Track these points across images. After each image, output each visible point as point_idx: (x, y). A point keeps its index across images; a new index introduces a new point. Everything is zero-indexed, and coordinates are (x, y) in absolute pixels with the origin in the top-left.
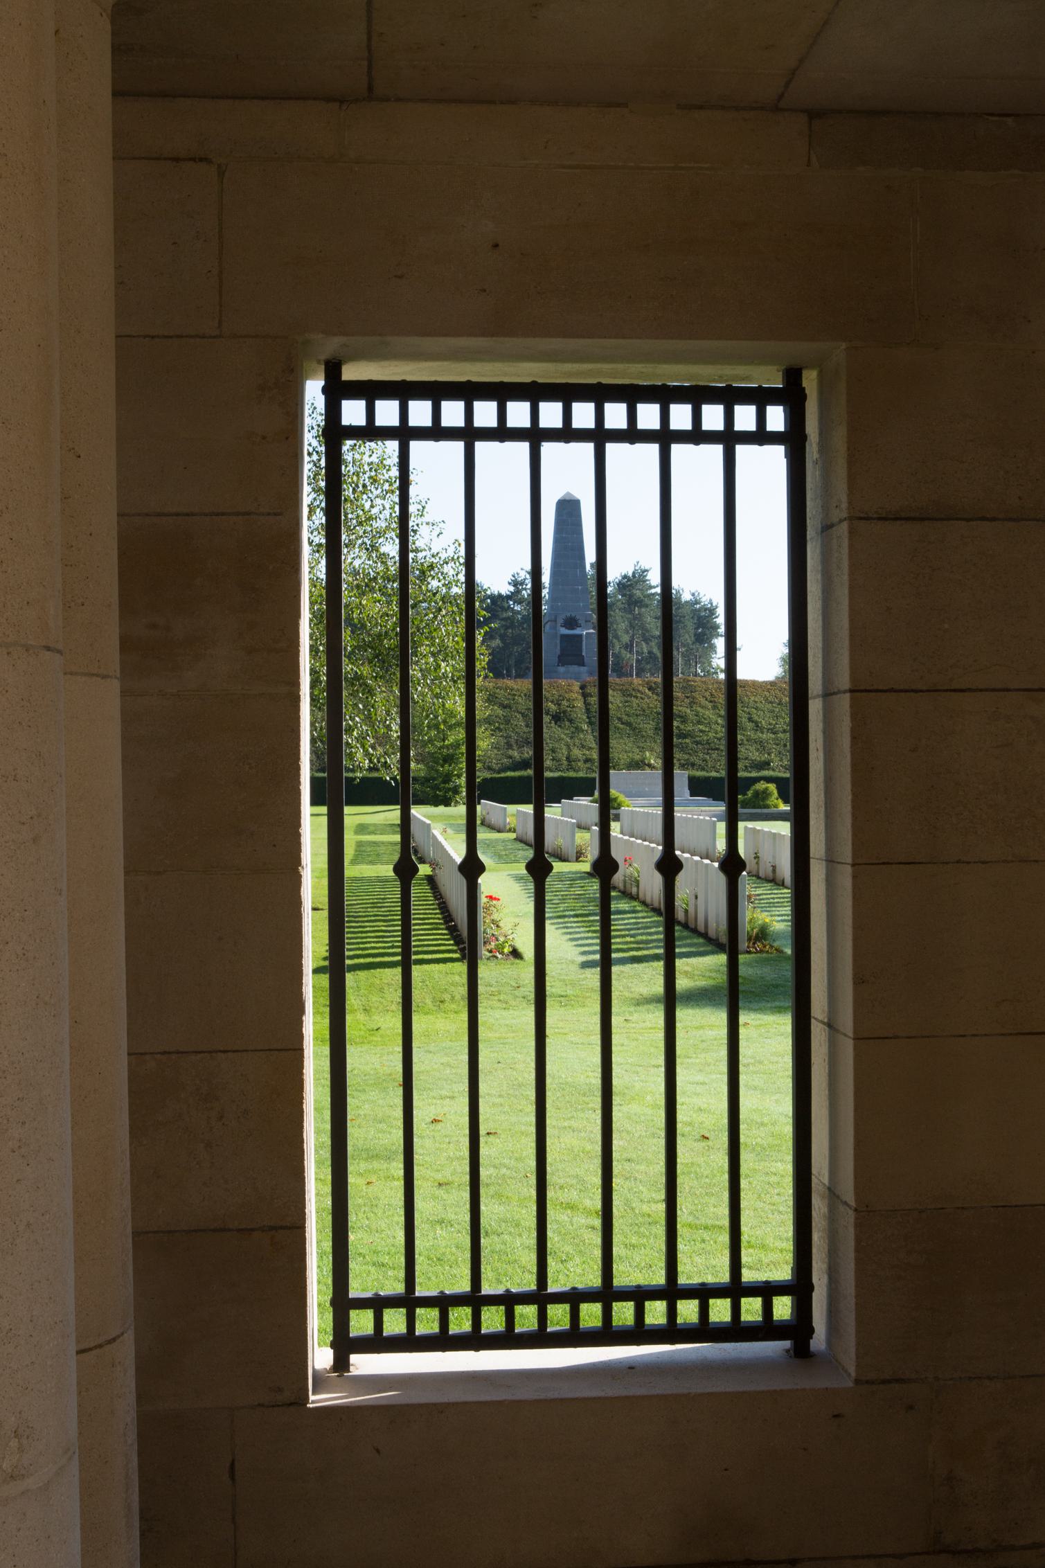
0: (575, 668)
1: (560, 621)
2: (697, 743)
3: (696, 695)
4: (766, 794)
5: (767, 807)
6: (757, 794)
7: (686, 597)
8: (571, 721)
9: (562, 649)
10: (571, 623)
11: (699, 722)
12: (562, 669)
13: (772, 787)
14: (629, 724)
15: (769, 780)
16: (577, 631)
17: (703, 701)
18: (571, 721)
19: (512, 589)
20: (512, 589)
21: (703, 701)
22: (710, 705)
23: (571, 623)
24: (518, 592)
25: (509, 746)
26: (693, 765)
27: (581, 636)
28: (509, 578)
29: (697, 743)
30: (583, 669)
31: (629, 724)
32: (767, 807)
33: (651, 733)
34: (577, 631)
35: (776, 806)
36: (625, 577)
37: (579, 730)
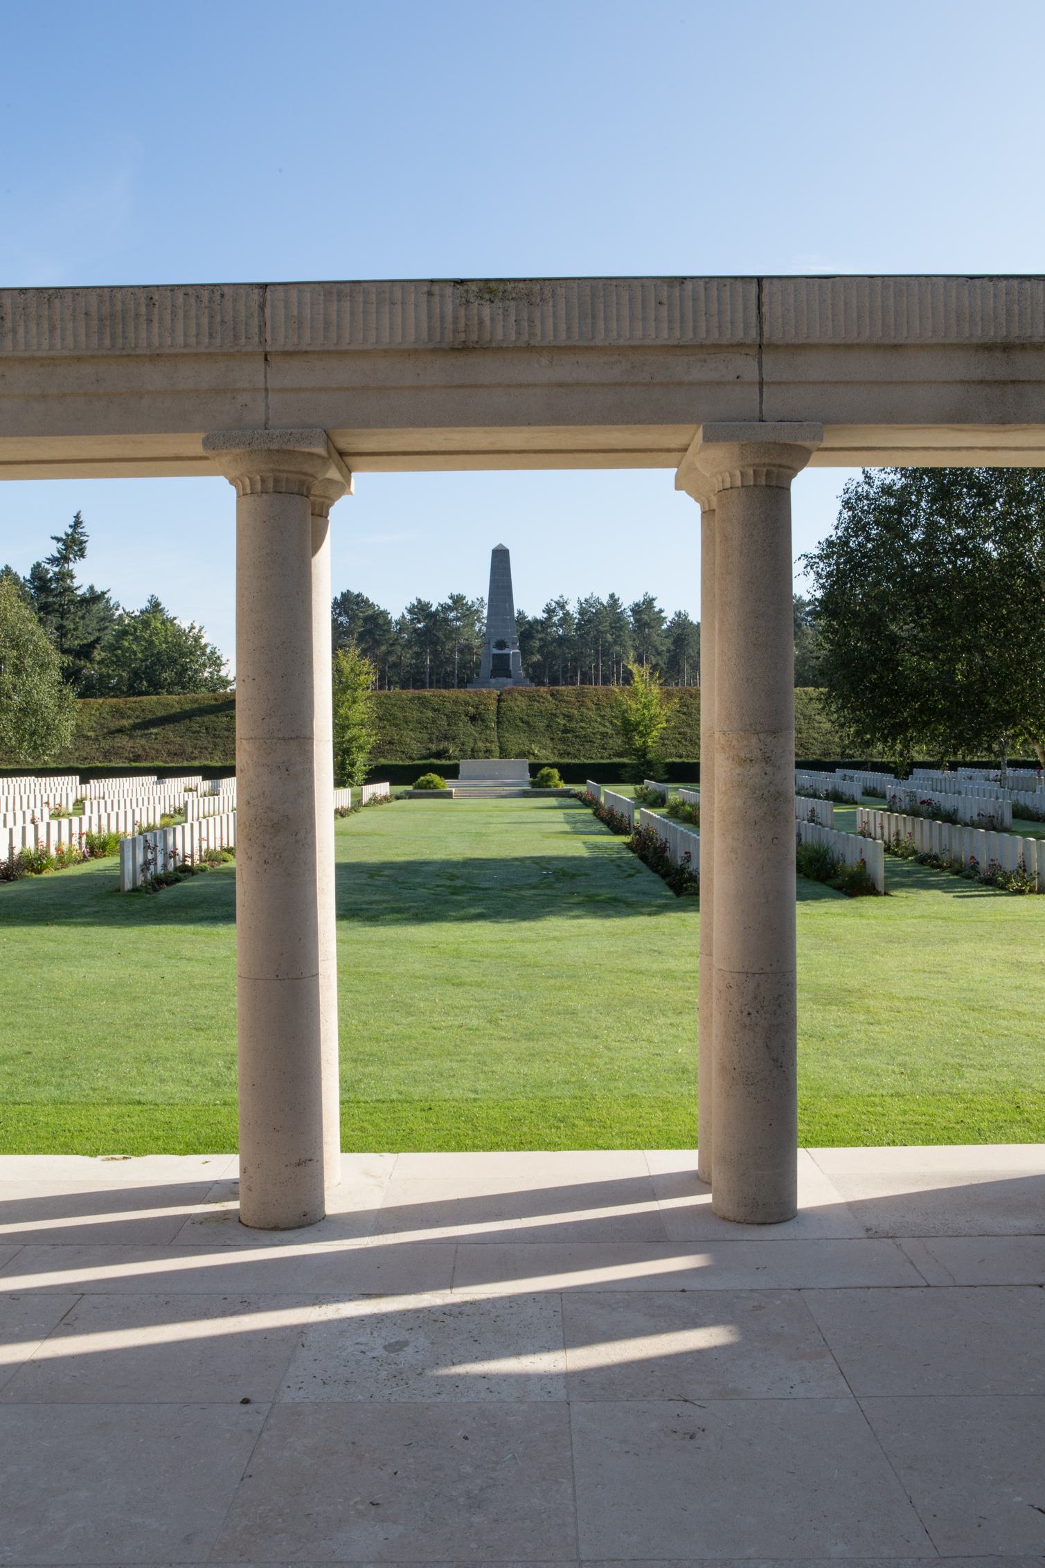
0: (504, 680)
1: (493, 643)
2: (577, 737)
3: (586, 700)
4: (548, 777)
5: (549, 786)
6: (542, 777)
7: (669, 615)
8: (483, 721)
9: (494, 666)
10: (501, 645)
11: (582, 721)
12: (493, 681)
13: (555, 772)
14: (527, 723)
15: (552, 766)
16: (505, 651)
17: (590, 704)
18: (483, 721)
19: (545, 615)
20: (545, 615)
21: (590, 704)
22: (594, 707)
23: (501, 645)
24: (549, 618)
25: (431, 740)
26: (569, 754)
27: (508, 655)
28: (543, 607)
29: (577, 737)
30: (510, 680)
31: (527, 723)
32: (549, 786)
33: (542, 729)
34: (505, 651)
35: (556, 786)
36: (637, 605)
37: (487, 727)
